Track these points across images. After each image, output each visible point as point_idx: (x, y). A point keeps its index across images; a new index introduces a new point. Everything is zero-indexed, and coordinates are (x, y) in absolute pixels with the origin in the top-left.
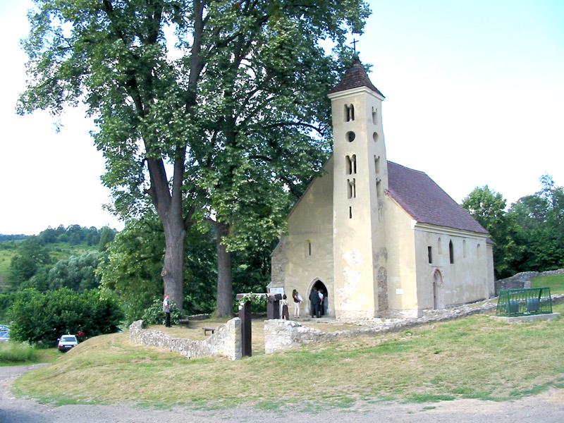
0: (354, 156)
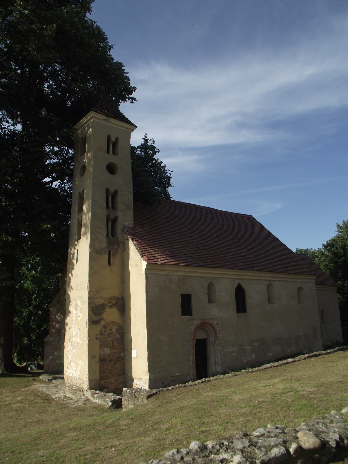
0: (116, 192)
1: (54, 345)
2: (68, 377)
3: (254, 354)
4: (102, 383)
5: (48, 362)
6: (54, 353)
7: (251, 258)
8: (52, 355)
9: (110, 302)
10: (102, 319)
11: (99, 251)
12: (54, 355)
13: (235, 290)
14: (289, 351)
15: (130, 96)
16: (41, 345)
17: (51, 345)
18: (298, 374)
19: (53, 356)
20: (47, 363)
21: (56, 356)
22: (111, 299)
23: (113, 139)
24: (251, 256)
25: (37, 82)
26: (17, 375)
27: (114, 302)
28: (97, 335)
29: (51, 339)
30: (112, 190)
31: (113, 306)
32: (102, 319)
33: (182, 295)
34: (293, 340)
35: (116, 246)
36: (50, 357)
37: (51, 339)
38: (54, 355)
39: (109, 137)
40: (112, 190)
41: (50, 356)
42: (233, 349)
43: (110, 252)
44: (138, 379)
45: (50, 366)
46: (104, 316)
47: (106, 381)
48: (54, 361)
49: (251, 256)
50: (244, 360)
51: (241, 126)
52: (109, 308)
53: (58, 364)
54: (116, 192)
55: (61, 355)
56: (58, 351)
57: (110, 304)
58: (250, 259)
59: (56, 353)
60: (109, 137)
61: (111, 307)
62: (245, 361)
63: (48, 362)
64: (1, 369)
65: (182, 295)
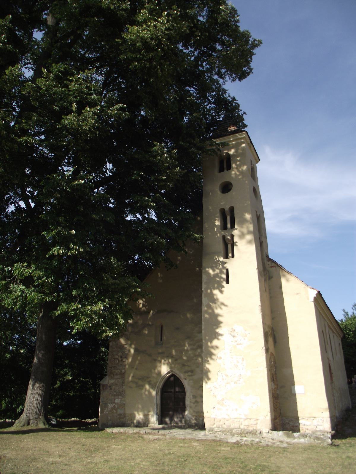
0: (232, 210)
1: (114, 389)
2: (215, 420)
5: (107, 412)
6: (114, 400)
8: (112, 403)
12: (114, 403)
17: (111, 389)
18: (83, 441)
19: (113, 404)
20: (105, 412)
21: (117, 404)
25: (109, 80)
29: (112, 381)
30: (227, 208)
36: (110, 406)
37: (112, 381)
38: (114, 403)
40: (227, 208)
41: (109, 403)
44: (307, 418)
45: (109, 418)
48: (115, 411)
51: (294, 219)
53: (120, 415)
55: (124, 402)
56: (120, 397)
59: (117, 401)
63: (107, 412)
64: (41, 421)
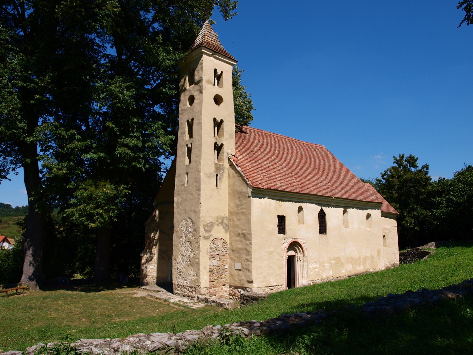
3: (331, 271)
4: (211, 290)
7: (330, 185)
9: (217, 221)
10: (211, 235)
11: (209, 175)
13: (319, 214)
14: (358, 269)
15: (158, 243)
16: (97, 56)
22: (218, 218)
23: (219, 73)
24: (330, 184)
26: (217, 57)
27: (220, 221)
28: (207, 249)
30: (218, 120)
31: (220, 225)
32: (211, 235)
33: (279, 217)
34: (361, 260)
35: (222, 171)
39: (216, 71)
40: (218, 120)
42: (316, 266)
43: (217, 175)
46: (212, 233)
47: (214, 289)
49: (330, 184)
50: (324, 275)
52: (216, 226)
54: (222, 121)
57: (217, 223)
58: (329, 187)
60: (216, 71)
61: (218, 225)
62: (325, 277)
65: (279, 217)
